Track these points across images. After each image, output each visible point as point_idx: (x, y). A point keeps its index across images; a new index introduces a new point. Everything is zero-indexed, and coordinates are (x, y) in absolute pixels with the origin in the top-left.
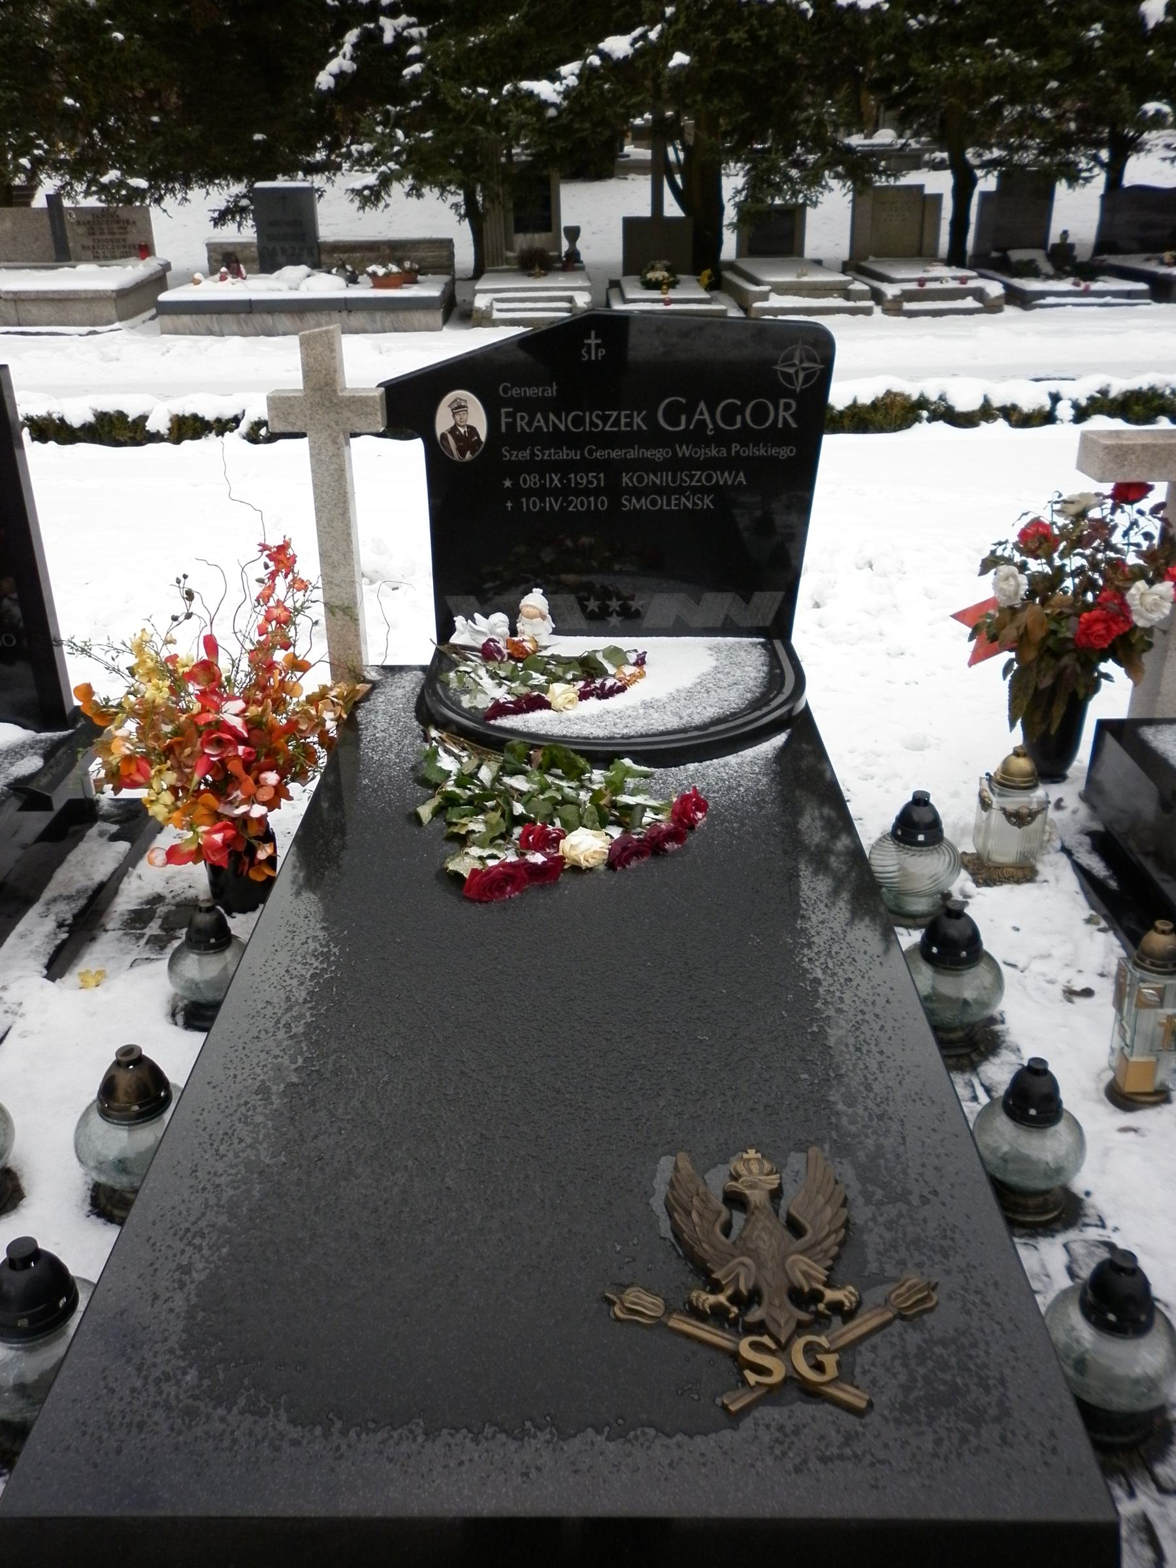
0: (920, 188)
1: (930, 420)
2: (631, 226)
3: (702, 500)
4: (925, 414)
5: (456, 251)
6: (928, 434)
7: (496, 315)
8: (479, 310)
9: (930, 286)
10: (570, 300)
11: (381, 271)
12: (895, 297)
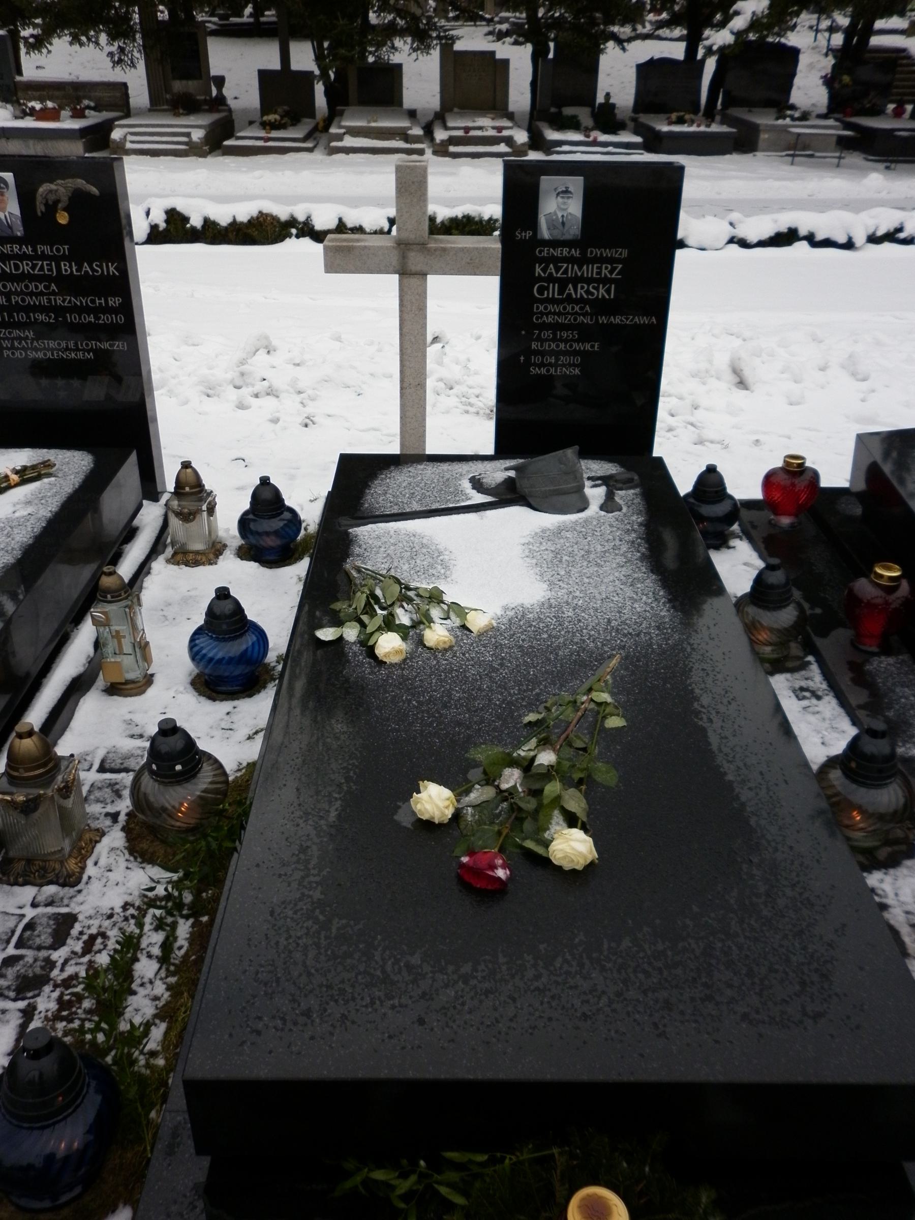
0: (493, 53)
1: (298, 237)
2: (264, 76)
3: (597, 289)
4: (294, 231)
5: (130, 92)
6: (802, 247)
7: (129, 146)
8: (115, 141)
9: (473, 133)
10: (188, 135)
11: (38, 106)
12: (442, 141)
